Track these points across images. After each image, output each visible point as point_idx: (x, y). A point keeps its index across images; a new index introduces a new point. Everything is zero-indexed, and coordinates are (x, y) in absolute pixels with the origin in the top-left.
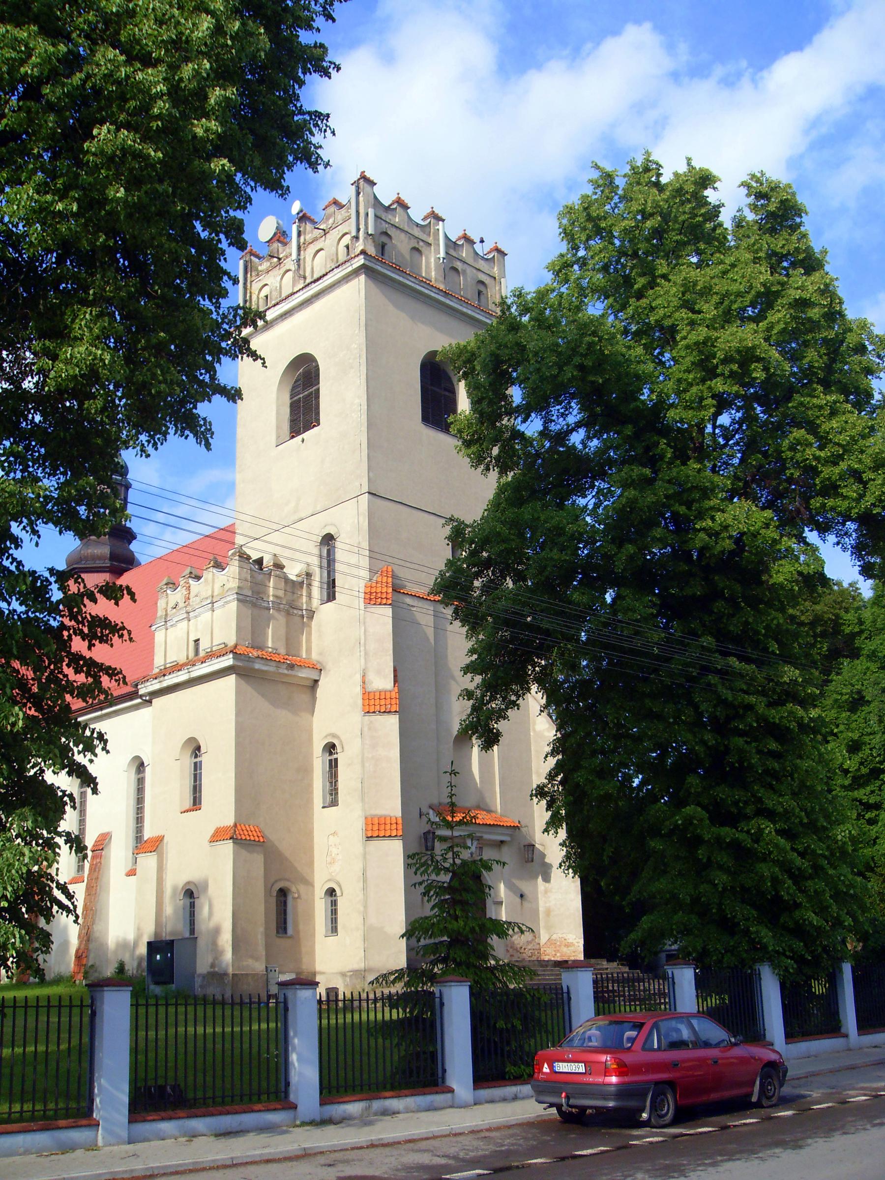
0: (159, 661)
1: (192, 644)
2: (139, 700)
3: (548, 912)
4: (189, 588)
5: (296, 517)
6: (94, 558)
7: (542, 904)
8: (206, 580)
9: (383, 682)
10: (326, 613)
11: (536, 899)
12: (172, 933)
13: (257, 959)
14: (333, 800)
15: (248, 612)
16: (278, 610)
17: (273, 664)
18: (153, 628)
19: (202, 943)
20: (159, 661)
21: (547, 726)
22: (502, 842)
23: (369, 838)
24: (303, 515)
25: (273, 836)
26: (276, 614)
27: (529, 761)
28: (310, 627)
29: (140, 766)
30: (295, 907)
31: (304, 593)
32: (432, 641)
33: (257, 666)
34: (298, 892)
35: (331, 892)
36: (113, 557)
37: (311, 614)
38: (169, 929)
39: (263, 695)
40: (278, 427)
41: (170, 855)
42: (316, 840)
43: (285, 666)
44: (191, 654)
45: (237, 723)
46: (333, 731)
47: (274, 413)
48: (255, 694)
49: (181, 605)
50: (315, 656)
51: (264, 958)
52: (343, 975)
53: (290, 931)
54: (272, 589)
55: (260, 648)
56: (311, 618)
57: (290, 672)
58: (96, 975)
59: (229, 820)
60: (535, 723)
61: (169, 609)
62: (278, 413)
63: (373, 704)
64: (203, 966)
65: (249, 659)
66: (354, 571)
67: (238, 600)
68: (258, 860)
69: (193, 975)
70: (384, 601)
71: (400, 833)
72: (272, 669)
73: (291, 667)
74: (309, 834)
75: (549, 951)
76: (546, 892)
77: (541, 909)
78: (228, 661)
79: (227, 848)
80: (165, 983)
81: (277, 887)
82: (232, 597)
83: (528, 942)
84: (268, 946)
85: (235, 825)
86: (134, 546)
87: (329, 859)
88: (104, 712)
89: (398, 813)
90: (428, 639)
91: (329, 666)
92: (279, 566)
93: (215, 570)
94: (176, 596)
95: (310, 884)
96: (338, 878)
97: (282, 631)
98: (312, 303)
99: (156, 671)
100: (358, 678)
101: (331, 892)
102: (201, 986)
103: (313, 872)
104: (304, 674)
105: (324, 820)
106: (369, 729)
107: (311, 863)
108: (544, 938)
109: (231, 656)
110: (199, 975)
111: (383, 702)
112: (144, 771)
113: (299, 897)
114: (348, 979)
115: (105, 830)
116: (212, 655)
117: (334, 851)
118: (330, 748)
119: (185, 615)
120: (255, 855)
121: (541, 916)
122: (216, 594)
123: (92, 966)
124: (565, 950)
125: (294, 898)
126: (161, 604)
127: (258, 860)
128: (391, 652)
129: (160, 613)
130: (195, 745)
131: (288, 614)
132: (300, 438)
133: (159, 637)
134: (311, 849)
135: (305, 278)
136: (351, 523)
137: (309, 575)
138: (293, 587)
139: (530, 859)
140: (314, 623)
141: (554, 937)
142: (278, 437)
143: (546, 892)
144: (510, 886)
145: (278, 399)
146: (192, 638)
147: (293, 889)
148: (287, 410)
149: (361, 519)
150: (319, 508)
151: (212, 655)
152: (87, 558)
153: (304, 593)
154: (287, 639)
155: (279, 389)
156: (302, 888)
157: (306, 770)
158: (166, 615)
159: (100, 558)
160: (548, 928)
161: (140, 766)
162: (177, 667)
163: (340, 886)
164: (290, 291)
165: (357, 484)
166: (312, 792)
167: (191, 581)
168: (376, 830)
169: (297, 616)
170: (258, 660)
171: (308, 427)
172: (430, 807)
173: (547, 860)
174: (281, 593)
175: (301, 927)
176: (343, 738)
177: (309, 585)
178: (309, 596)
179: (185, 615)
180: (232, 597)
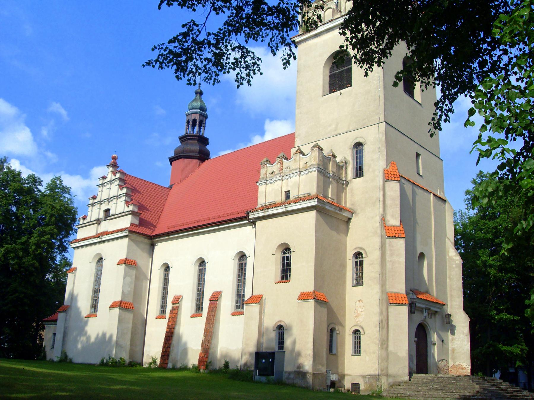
0: (261, 201)
1: (284, 193)
2: (247, 222)
3: (453, 350)
4: (282, 164)
5: (336, 133)
6: (190, 151)
7: (450, 347)
8: (295, 160)
9: (394, 220)
10: (357, 185)
11: (448, 343)
12: (266, 348)
13: (323, 366)
14: (359, 281)
15: (322, 178)
16: (334, 179)
17: (334, 207)
18: (258, 184)
19: (287, 355)
20: (261, 201)
21: (455, 254)
22: (436, 312)
23: (391, 304)
24: (341, 132)
25: (329, 300)
26: (333, 181)
27: (446, 272)
28: (346, 190)
29: (242, 256)
30: (337, 338)
31: (344, 173)
32: (411, 203)
33: (327, 207)
34: (339, 331)
35: (356, 332)
36: (200, 152)
37: (347, 183)
38: (264, 346)
39: (327, 223)
40: (324, 87)
41: (266, 306)
42: (347, 304)
43: (338, 209)
44: (284, 198)
45: (316, 236)
46: (360, 246)
47: (321, 79)
48: (324, 222)
49: (277, 172)
50: (348, 206)
51: (325, 366)
52: (364, 377)
53: (334, 352)
54: (331, 168)
55: (326, 197)
56: (347, 185)
57: (340, 212)
58: (211, 367)
59: (310, 288)
60: (449, 252)
61: (268, 174)
62: (323, 79)
63: (389, 232)
64: (288, 368)
65: (324, 203)
66: (375, 161)
67: (318, 171)
68: (324, 310)
69: (282, 372)
70: (396, 179)
71: (407, 302)
72: (333, 210)
73: (341, 209)
74: (343, 300)
75: (453, 371)
76: (452, 340)
77: (450, 349)
78: (314, 203)
79: (311, 304)
80: (268, 375)
81: (330, 327)
82: (314, 169)
83: (445, 366)
84: (327, 359)
85: (314, 292)
86: (208, 147)
87: (355, 314)
88: (220, 227)
89: (404, 292)
90: (409, 202)
91: (359, 211)
92: (334, 156)
93: (301, 155)
94: (275, 167)
95: (343, 326)
96: (362, 325)
97: (335, 190)
98: (333, 30)
99: (259, 206)
100: (378, 218)
101: (356, 332)
102: (287, 378)
103: (345, 321)
104: (346, 214)
105: (352, 294)
106: (389, 245)
107: (344, 315)
108: (451, 364)
109: (316, 200)
110: (286, 372)
111: (396, 232)
112: (169, 270)
113: (339, 334)
114: (367, 380)
115: (218, 289)
116: (298, 200)
117: (360, 310)
118: (358, 255)
119: (281, 178)
120: (323, 308)
121: (450, 352)
122: (301, 167)
123: (210, 362)
124: (461, 371)
125: (337, 334)
126: (263, 171)
127: (324, 310)
128: (399, 206)
129: (262, 176)
130: (284, 247)
131: (338, 182)
132: (339, 92)
133: (261, 188)
134: (345, 307)
135: (341, 12)
136: (374, 138)
137: (346, 163)
138: (340, 167)
139: (448, 323)
140: (348, 188)
141: (456, 363)
142: (323, 92)
143: (452, 340)
144: (439, 336)
145: (324, 72)
146: (285, 189)
147: (337, 329)
148: (328, 78)
149: (381, 135)
150: (351, 129)
151: (298, 200)
152: (186, 151)
153: (344, 173)
154: (337, 195)
155: (324, 67)
156: (340, 327)
157: (343, 266)
158: (266, 177)
159: (193, 151)
160: (453, 359)
161: (242, 256)
162: (273, 205)
163: (363, 329)
164: (331, 18)
165: (377, 117)
166: (345, 278)
167: (284, 160)
168: (391, 300)
169: (342, 185)
170: (327, 204)
171: (341, 87)
172: (411, 290)
173: (453, 323)
174: (335, 170)
175: (339, 350)
176: (367, 250)
177: (346, 168)
178: (346, 173)
179: (281, 178)
180: (314, 169)
